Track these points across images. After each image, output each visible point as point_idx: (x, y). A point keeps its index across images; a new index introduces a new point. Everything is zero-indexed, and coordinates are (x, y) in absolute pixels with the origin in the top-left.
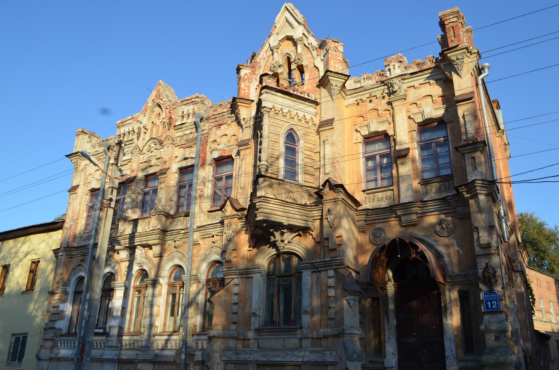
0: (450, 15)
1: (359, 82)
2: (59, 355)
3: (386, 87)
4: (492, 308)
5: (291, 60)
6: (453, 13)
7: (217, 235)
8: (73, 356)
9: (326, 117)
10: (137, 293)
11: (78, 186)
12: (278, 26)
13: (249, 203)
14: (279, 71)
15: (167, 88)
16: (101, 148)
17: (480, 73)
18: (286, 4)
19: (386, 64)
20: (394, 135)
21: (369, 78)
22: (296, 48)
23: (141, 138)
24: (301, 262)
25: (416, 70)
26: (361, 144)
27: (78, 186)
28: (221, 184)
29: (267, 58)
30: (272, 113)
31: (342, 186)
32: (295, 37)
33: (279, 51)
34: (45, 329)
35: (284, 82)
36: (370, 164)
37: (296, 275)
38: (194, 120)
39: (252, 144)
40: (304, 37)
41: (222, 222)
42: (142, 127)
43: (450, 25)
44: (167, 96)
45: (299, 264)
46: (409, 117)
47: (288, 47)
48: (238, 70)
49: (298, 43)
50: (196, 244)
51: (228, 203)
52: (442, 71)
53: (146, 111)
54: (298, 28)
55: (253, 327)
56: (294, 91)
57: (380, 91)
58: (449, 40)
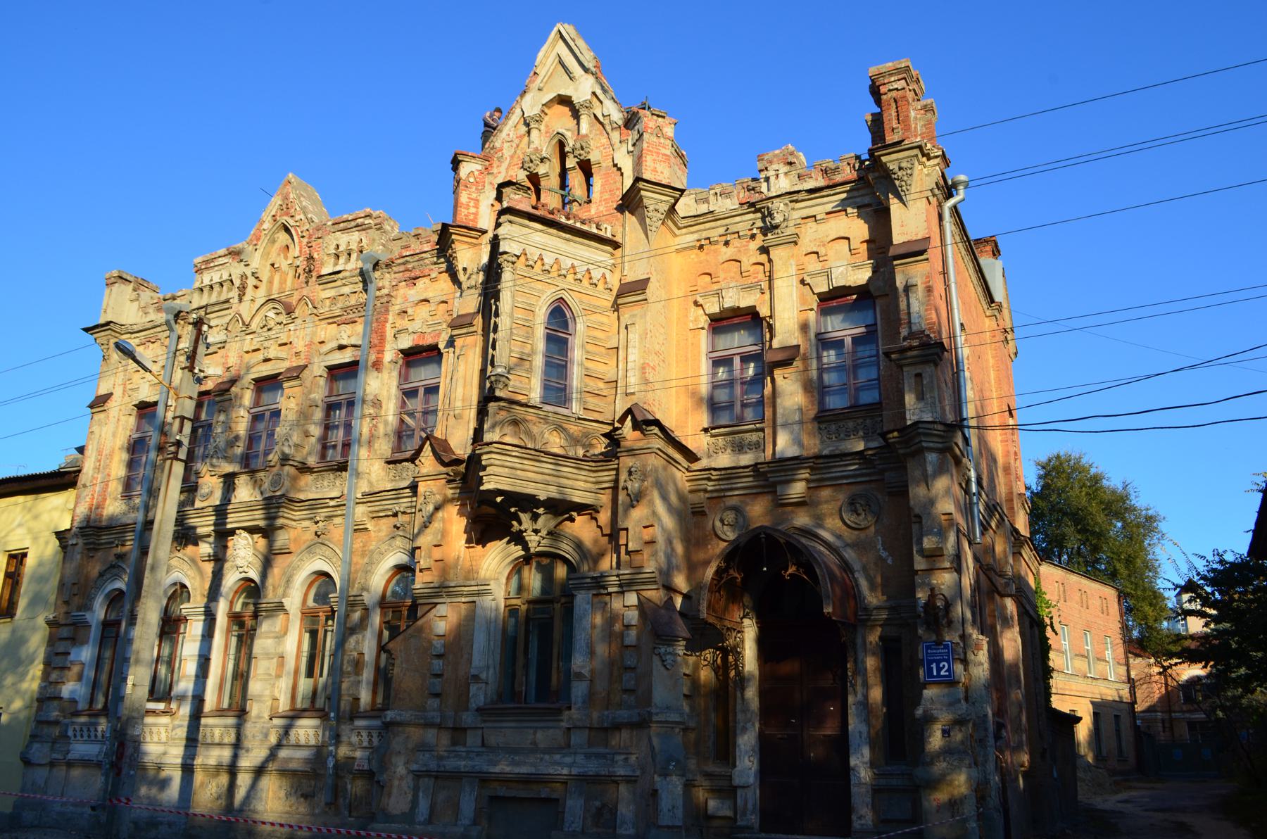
0: (891, 75)
1: (706, 201)
2: (70, 756)
3: (759, 215)
4: (939, 675)
5: (567, 149)
6: (898, 71)
7: (404, 513)
8: (100, 758)
9: (632, 275)
10: (235, 628)
11: (109, 395)
12: (542, 71)
13: (469, 451)
14: (542, 170)
15: (306, 191)
16: (160, 315)
17: (949, 195)
18: (559, 26)
19: (760, 166)
20: (771, 317)
21: (725, 194)
22: (578, 124)
23: (247, 297)
24: (572, 576)
25: (821, 182)
26: (704, 332)
27: (109, 395)
28: (416, 404)
29: (517, 141)
30: (520, 264)
31: (657, 423)
32: (575, 100)
33: (543, 127)
34: (39, 700)
35: (548, 199)
36: (722, 373)
37: (563, 600)
38: (360, 264)
39: (479, 321)
40: (595, 99)
41: (414, 488)
42: (249, 274)
43: (890, 94)
44: (304, 210)
45: (568, 579)
46: (802, 282)
47: (560, 120)
48: (456, 163)
49: (582, 111)
50: (360, 530)
51: (427, 446)
52: (872, 190)
53: (258, 239)
54: (582, 79)
55: (473, 705)
56: (568, 218)
57: (749, 221)
58: (887, 127)
